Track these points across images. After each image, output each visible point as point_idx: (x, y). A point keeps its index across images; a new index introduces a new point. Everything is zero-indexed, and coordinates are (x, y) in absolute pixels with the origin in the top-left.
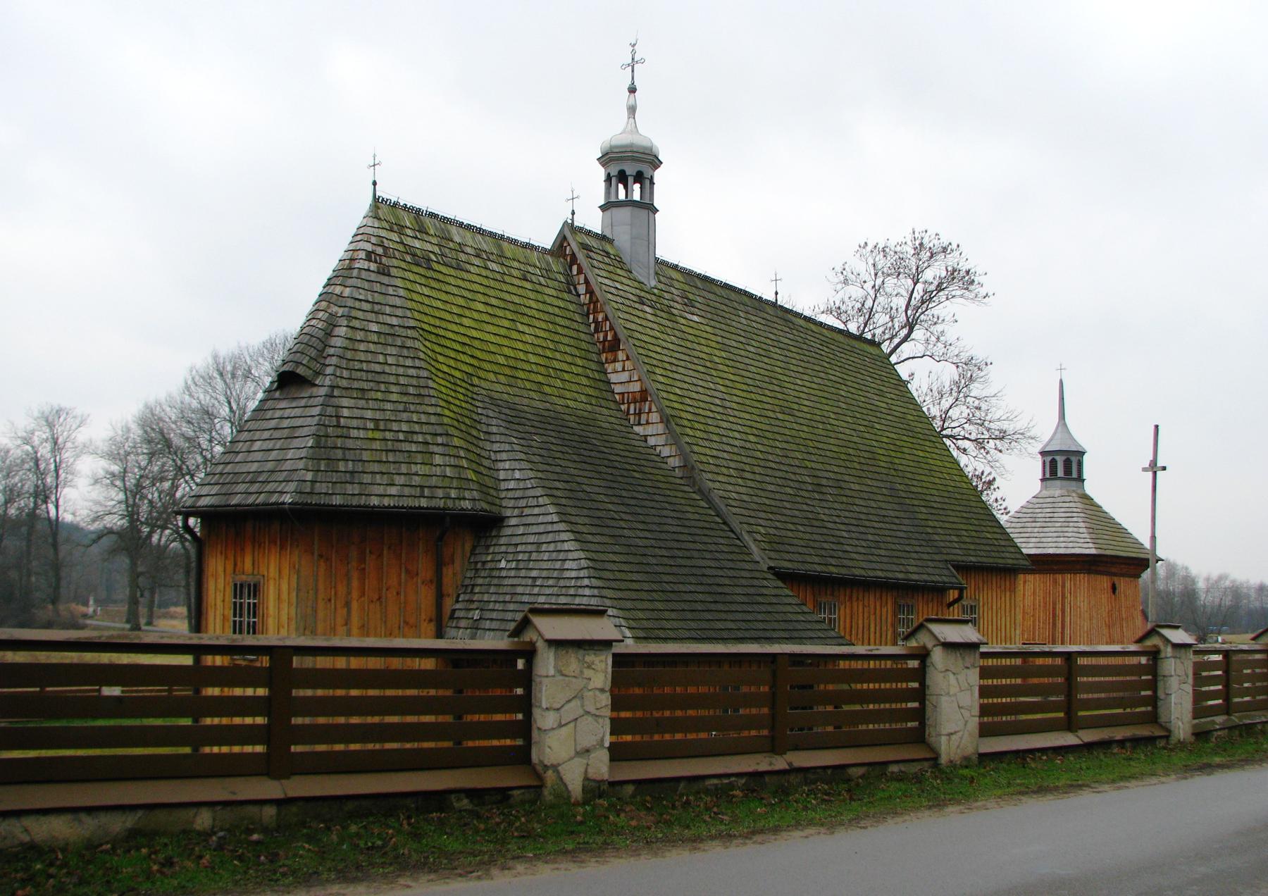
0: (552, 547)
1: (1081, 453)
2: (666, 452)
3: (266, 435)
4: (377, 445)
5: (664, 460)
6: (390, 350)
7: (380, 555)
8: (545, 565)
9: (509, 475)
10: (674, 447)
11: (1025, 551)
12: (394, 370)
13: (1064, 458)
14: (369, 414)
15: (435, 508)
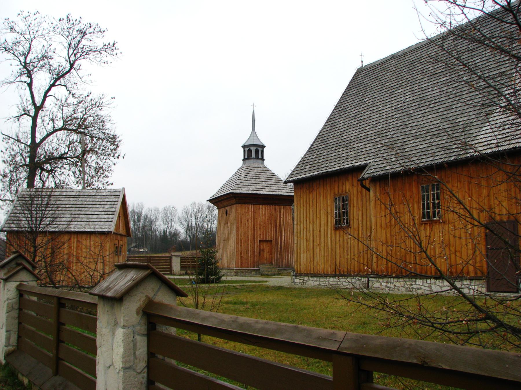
1: (263, 147)
13: (255, 148)
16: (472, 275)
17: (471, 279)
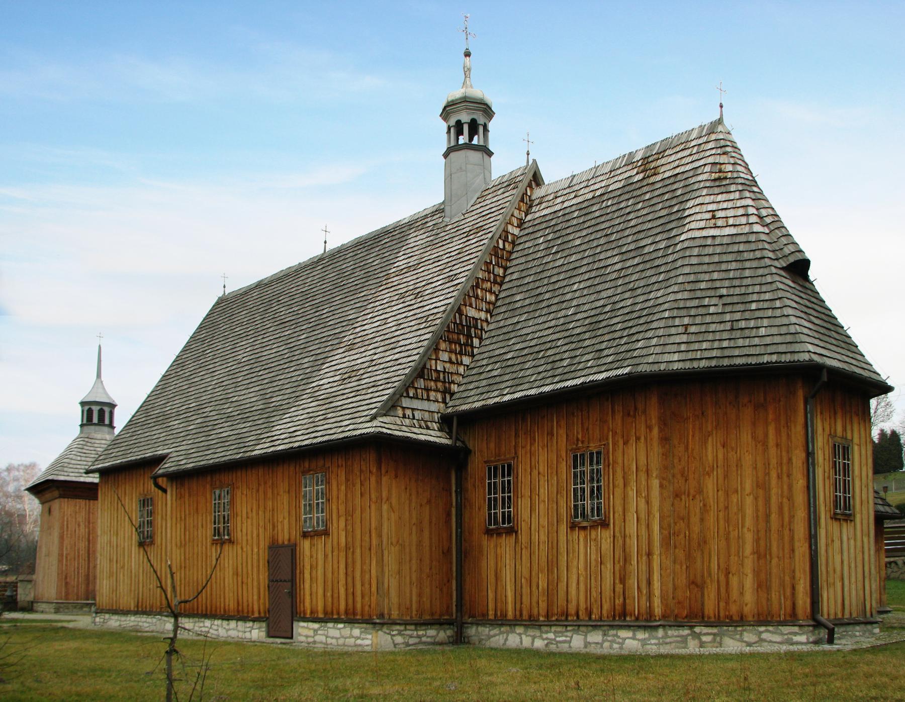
1: (112, 406)
13: (99, 408)
16: (256, 615)
17: (254, 620)
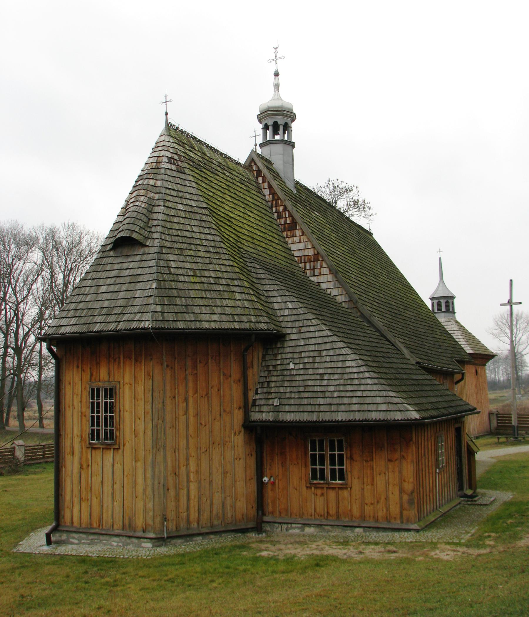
0: (331, 353)
2: (334, 292)
3: (112, 281)
4: (198, 287)
5: (334, 298)
6: (193, 223)
7: (207, 363)
8: (329, 365)
9: (283, 306)
10: (340, 289)
11: (468, 352)
12: (198, 236)
13: (445, 300)
14: (188, 265)
15: (244, 329)
